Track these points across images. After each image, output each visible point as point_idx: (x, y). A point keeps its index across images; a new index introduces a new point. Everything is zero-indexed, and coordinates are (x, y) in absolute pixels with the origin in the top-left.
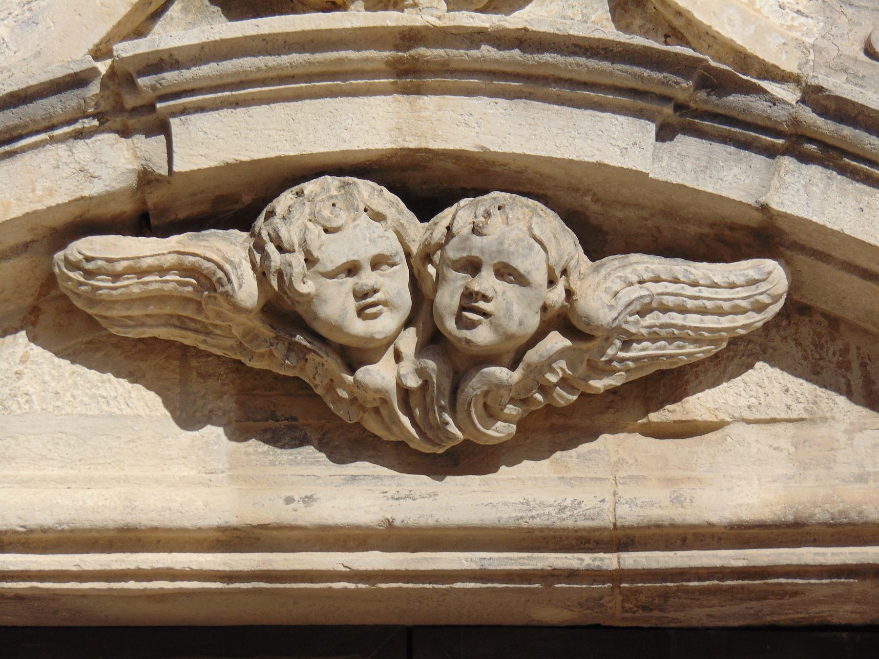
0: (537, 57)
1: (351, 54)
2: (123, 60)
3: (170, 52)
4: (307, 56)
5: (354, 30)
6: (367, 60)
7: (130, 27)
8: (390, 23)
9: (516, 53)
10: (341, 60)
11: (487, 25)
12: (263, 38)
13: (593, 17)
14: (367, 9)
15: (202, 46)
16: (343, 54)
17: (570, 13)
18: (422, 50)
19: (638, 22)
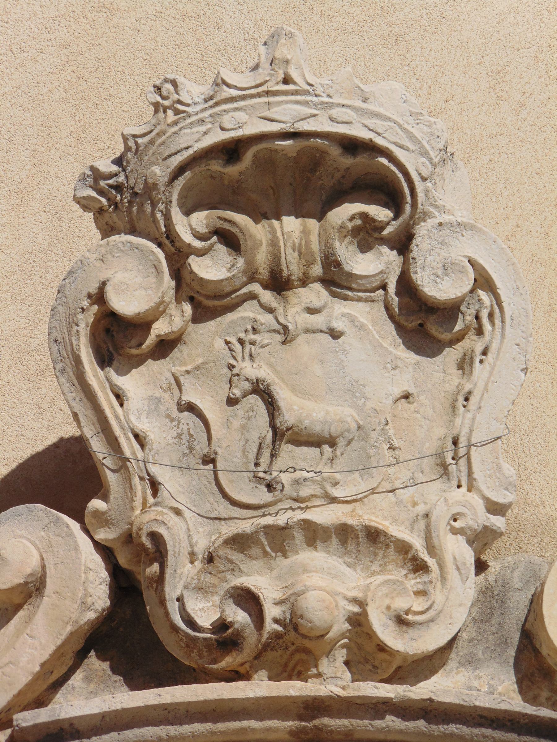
0: (442, 728)
1: (254, 724)
2: (23, 730)
3: (71, 722)
4: (209, 726)
5: (257, 699)
6: (269, 729)
7: (31, 697)
8: (293, 693)
9: (421, 724)
10: (243, 730)
11: (392, 695)
12: (165, 707)
13: (500, 689)
14: (270, 679)
15: (103, 716)
16: (245, 723)
17: (476, 684)
18: (326, 721)
19: (545, 694)
